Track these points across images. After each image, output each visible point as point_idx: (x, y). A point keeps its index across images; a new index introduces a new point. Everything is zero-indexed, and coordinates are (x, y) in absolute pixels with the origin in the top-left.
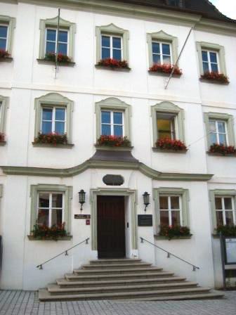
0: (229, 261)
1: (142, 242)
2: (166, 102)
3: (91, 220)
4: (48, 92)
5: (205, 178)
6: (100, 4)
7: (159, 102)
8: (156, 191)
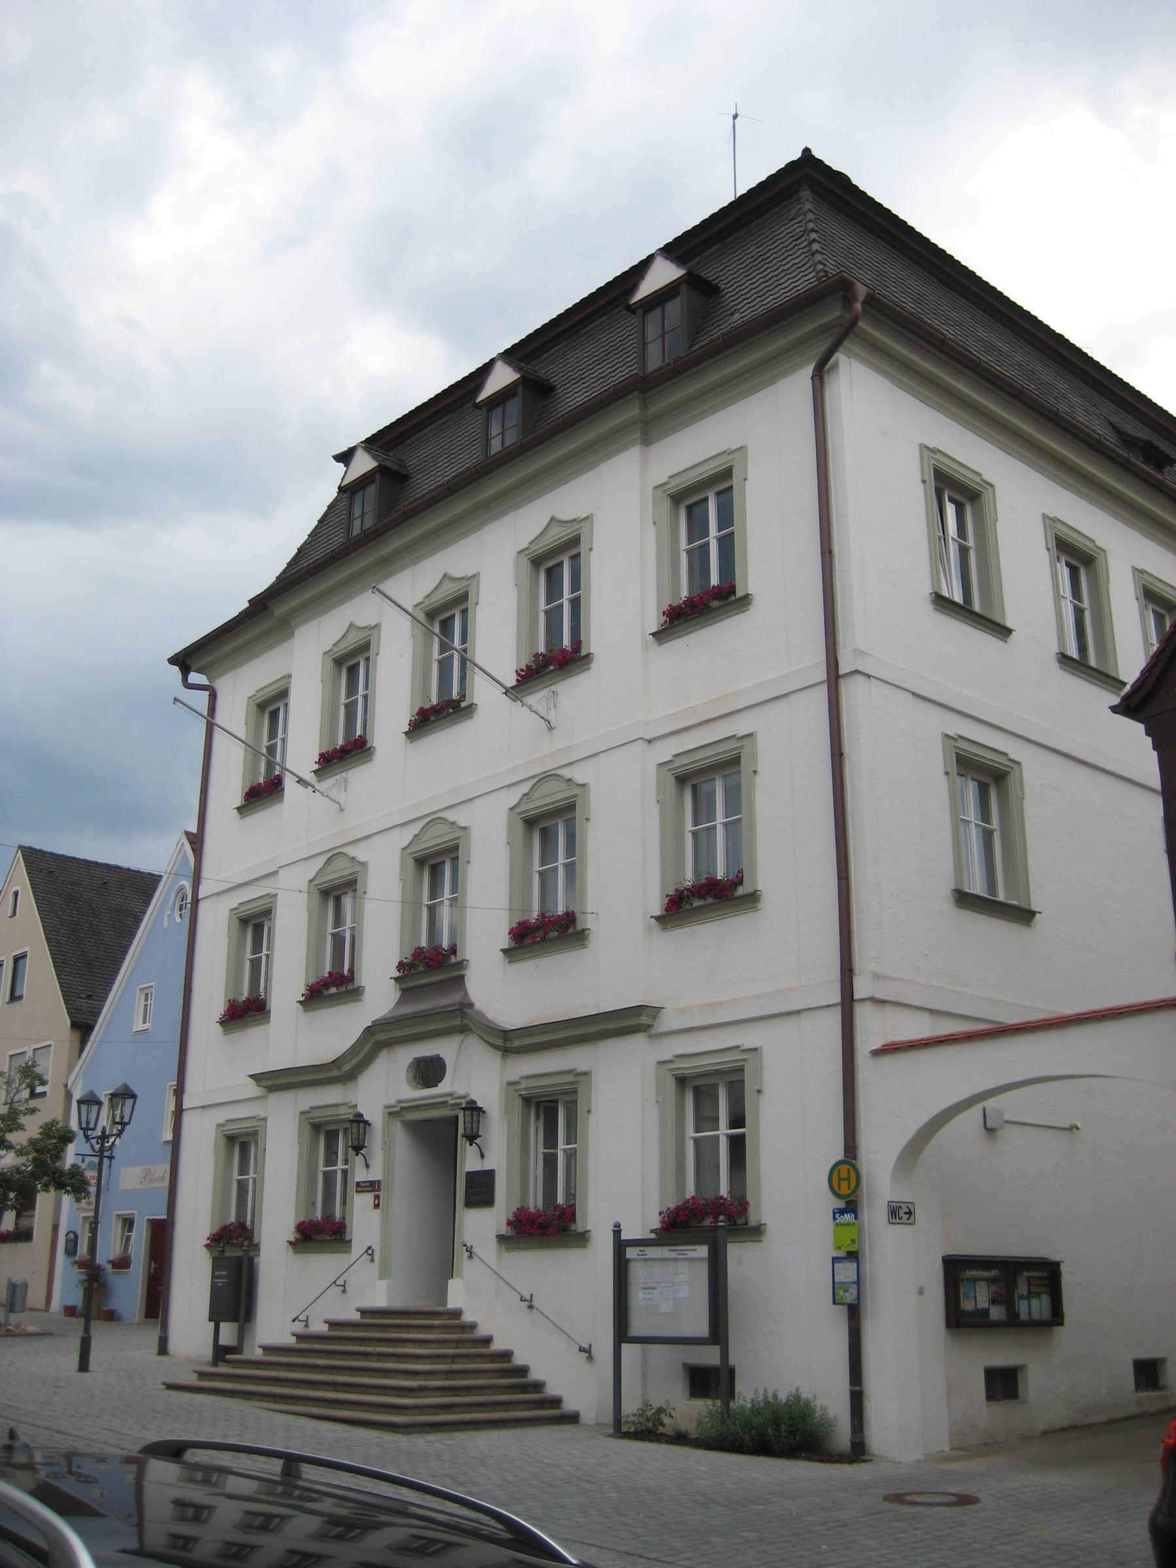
0: (636, 1330)
1: (470, 1257)
2: (546, 777)
3: (381, 1193)
4: (329, 855)
5: (631, 1022)
6: (560, 453)
7: (525, 788)
8: (305, 1116)
